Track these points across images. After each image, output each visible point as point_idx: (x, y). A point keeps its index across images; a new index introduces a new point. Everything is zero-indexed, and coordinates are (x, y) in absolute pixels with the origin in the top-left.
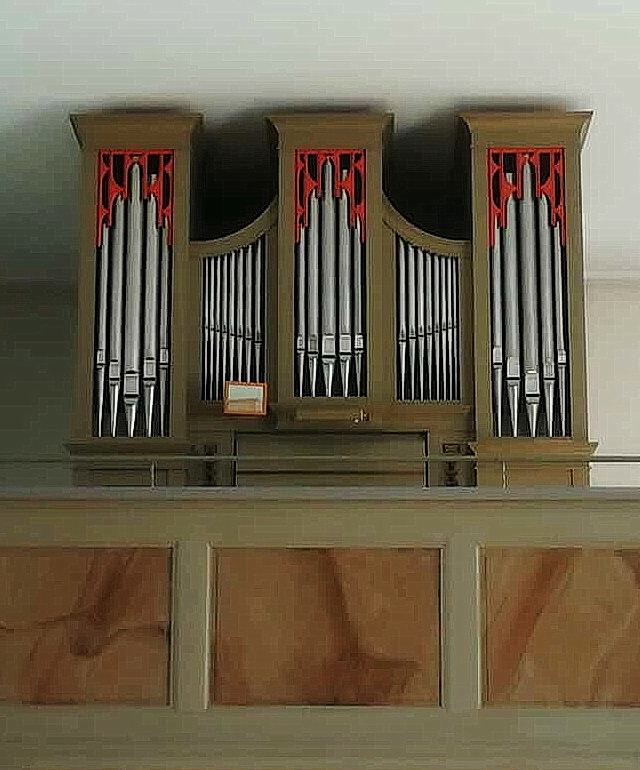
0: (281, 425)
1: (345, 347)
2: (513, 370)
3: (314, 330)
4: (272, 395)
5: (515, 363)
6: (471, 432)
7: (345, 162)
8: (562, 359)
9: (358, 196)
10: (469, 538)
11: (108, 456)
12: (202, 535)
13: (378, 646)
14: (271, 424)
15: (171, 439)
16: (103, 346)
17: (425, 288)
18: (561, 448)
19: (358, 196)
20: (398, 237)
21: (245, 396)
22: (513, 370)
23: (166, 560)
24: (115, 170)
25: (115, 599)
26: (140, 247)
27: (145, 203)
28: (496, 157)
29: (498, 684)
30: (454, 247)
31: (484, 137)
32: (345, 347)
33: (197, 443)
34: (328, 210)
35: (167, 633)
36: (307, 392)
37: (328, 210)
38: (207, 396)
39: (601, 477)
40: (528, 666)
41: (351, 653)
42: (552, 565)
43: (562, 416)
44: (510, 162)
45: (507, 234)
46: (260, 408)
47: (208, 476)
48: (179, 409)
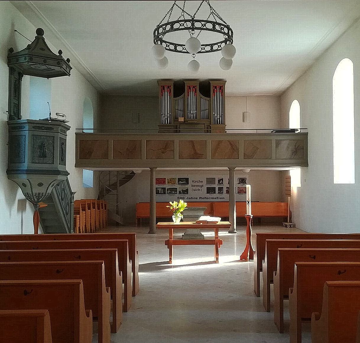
0: (186, 122)
1: (194, 112)
2: (216, 115)
3: (190, 110)
4: (185, 119)
5: (216, 115)
6: (210, 123)
7: (194, 87)
8: (222, 114)
9: (196, 92)
10: (210, 139)
11: (163, 128)
12: (177, 139)
13: (198, 152)
14: (185, 122)
15: (171, 125)
16: (162, 112)
17: (204, 101)
18: (221, 126)
19: (196, 92)
20: (201, 97)
21: (181, 119)
22: (216, 115)
23: (173, 141)
24: (163, 88)
25: (167, 147)
26: (167, 100)
27: (167, 93)
28: (214, 87)
29: (213, 157)
30: (208, 99)
31: (212, 84)
32: (194, 112)
33: (175, 127)
34: (192, 94)
35: (173, 151)
36: (189, 118)
37: (192, 94)
38: (176, 119)
39: (228, 132)
40: (217, 155)
41: (196, 153)
42: (220, 142)
43: (223, 123)
44: (216, 87)
45: (216, 97)
46: (219, 233)
47: (176, 132)
48: (172, 120)
